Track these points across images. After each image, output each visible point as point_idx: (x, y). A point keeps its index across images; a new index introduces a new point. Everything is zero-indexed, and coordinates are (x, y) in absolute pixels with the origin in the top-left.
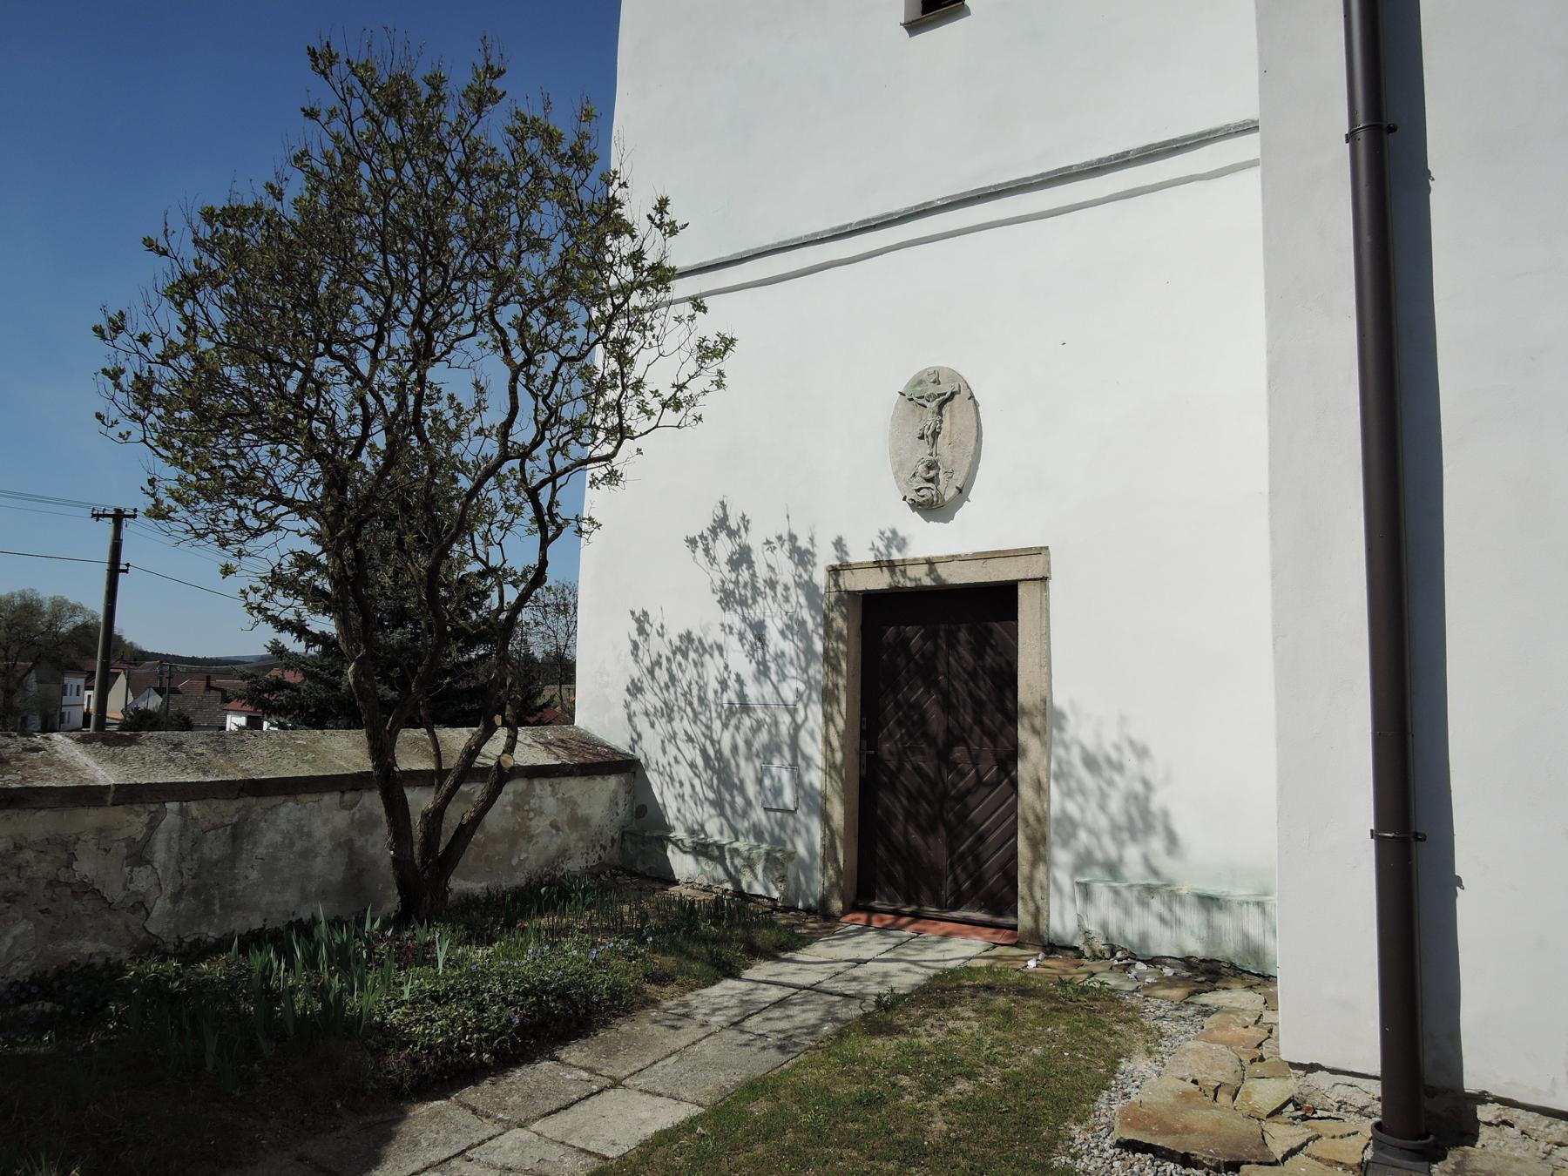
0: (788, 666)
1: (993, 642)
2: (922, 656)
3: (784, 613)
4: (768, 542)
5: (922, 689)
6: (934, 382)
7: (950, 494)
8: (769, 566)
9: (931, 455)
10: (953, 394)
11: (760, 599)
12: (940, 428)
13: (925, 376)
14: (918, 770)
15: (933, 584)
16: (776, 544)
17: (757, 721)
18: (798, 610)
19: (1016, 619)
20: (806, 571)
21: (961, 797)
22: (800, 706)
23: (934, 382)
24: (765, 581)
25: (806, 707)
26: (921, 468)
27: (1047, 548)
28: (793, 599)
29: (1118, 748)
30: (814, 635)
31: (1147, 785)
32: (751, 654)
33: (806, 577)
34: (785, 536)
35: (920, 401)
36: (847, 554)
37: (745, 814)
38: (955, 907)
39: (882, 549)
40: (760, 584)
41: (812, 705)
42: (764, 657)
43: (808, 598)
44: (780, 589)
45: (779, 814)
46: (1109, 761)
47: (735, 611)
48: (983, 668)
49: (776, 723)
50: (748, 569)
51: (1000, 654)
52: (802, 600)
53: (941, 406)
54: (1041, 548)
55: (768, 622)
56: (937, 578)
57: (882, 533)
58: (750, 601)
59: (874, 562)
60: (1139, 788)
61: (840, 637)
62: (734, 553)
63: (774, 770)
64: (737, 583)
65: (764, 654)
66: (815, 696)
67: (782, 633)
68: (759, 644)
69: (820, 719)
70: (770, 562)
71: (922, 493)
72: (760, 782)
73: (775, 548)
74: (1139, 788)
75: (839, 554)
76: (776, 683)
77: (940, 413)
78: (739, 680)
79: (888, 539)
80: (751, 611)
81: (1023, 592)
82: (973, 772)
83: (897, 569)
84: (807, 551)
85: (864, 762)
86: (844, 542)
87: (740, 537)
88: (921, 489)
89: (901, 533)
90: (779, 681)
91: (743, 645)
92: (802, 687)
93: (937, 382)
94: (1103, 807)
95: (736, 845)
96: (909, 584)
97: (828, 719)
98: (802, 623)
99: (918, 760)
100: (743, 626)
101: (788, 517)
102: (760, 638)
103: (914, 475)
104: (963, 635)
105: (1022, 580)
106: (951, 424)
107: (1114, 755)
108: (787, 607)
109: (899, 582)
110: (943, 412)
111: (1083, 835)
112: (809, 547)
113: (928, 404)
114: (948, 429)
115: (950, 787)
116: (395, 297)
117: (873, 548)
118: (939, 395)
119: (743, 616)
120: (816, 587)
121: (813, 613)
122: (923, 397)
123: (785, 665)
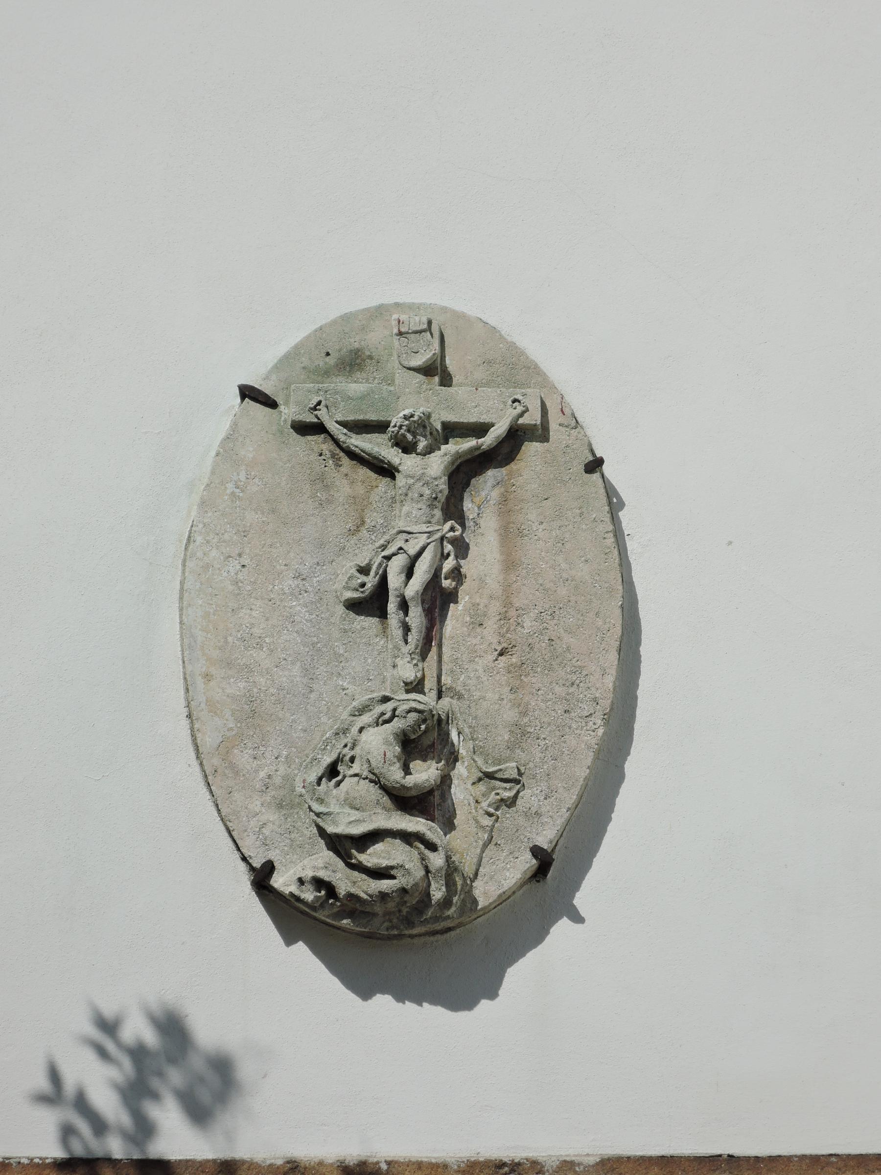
6: (427, 370)
9: (416, 687)
12: (457, 574)
23: (427, 370)
71: (372, 857)
103: (332, 771)
106: (510, 564)
110: (468, 506)
113: (407, 463)
114: (494, 583)
116: (433, 885)
118: (451, 430)
122: (380, 427)
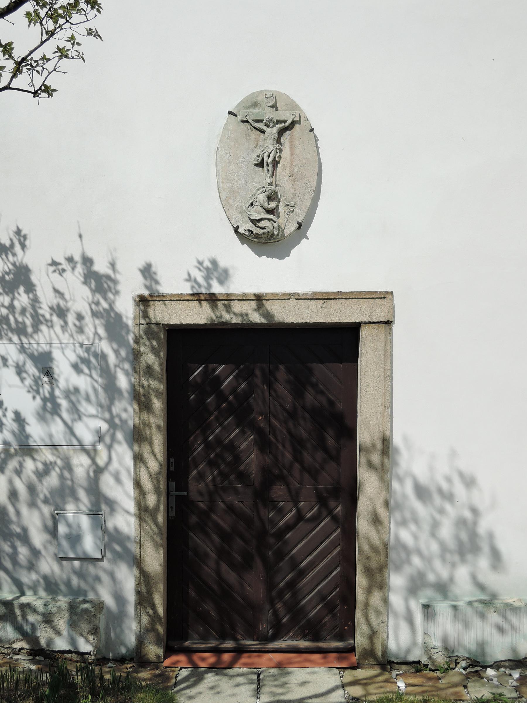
0: (84, 403)
1: (314, 380)
2: (237, 396)
3: (77, 345)
4: (54, 263)
5: (237, 431)
6: (272, 107)
7: (290, 228)
8: (56, 291)
9: (271, 184)
10: (293, 123)
11: (44, 328)
12: (280, 157)
13: (260, 99)
14: (231, 508)
15: (263, 321)
16: (65, 265)
17: (45, 464)
18: (97, 341)
19: (357, 361)
20: (105, 299)
21: (280, 534)
22: (101, 447)
23: (272, 107)
24: (52, 308)
25: (110, 448)
26: (262, 198)
27: (391, 293)
28: (89, 330)
29: (449, 480)
30: (118, 370)
31: (475, 511)
32: (35, 389)
33: (105, 305)
34: (77, 258)
35: (257, 125)
36: (157, 282)
37: (31, 567)
38: (275, 637)
39: (201, 280)
40: (45, 311)
41: (116, 446)
42: (52, 393)
43: (108, 328)
44: (71, 318)
45: (77, 564)
46: (440, 491)
47: (10, 340)
48: (304, 407)
49: (68, 466)
50: (27, 292)
51: (322, 393)
52: (101, 331)
53: (281, 132)
54: (386, 292)
55: (56, 354)
56: (267, 315)
57: (201, 263)
58: (30, 330)
59: (192, 295)
60: (468, 514)
61: (149, 371)
62: (8, 274)
63: (70, 516)
64: (11, 308)
65: (53, 389)
66: (119, 436)
67: (76, 367)
68: (46, 379)
69: (129, 462)
70: (57, 287)
72: (53, 532)
73: (64, 270)
74: (468, 514)
75: (148, 283)
76: (69, 422)
77: (279, 141)
78: (19, 418)
79: (207, 269)
80: (32, 341)
81: (365, 333)
82: (294, 512)
83: (220, 304)
84: (108, 277)
85: (173, 504)
86: (153, 269)
87: (14, 255)
88: (262, 219)
89: (222, 263)
90: (73, 420)
91: (22, 380)
92: (104, 426)
93: (274, 107)
94: (433, 535)
95: (24, 600)
96: (235, 320)
97: (138, 458)
98: (102, 357)
99: (231, 498)
100: (22, 358)
101: (80, 236)
102: (49, 373)
104: (282, 373)
105: (366, 323)
106: (292, 154)
107: (445, 486)
108: (81, 338)
109: (221, 317)
111: (416, 561)
112: (110, 272)
113: (268, 130)
115: (268, 527)
117: (189, 278)
118: (278, 122)
119: (22, 347)
120: (119, 317)
121: (115, 346)
122: (262, 121)
123: (79, 401)
